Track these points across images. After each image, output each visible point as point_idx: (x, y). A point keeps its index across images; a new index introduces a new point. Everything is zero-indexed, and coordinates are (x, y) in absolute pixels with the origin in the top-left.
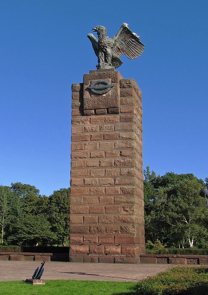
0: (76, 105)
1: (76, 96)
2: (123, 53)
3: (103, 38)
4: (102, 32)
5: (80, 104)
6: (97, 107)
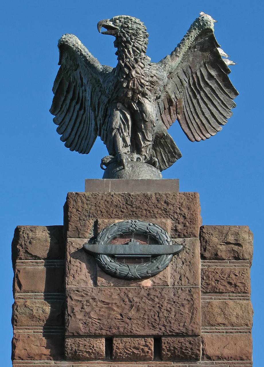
0: (35, 311)
1: (32, 275)
2: (174, 117)
3: (136, 61)
4: (134, 38)
5: (48, 309)
6: (122, 330)
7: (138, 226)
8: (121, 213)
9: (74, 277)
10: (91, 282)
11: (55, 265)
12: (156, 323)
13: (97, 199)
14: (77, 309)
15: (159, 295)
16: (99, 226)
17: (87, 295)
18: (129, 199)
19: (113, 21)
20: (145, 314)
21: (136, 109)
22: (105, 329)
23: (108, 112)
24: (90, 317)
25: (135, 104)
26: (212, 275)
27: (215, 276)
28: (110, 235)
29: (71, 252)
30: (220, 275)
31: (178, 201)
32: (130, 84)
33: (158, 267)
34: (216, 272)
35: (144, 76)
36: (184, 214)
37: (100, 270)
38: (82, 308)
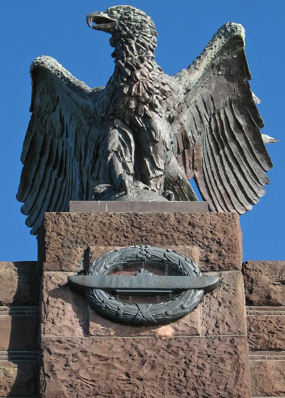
3: (142, 60)
4: (138, 31)
5: (13, 371)
7: (151, 252)
8: (123, 238)
9: (53, 323)
10: (80, 330)
11: (24, 313)
12: (181, 385)
13: (88, 220)
14: (59, 367)
15: (185, 347)
16: (92, 254)
17: (74, 347)
18: (136, 219)
19: (108, 13)
20: (163, 372)
21: (141, 125)
22: (102, 394)
23: (99, 150)
24: (79, 377)
25: (140, 119)
26: (263, 325)
27: (268, 327)
28: (109, 264)
29: (49, 290)
30: (276, 326)
31: (208, 222)
32: (133, 90)
33: (182, 306)
34: (269, 321)
35: (153, 81)
36: (219, 239)
37: (93, 313)
38: (66, 365)
